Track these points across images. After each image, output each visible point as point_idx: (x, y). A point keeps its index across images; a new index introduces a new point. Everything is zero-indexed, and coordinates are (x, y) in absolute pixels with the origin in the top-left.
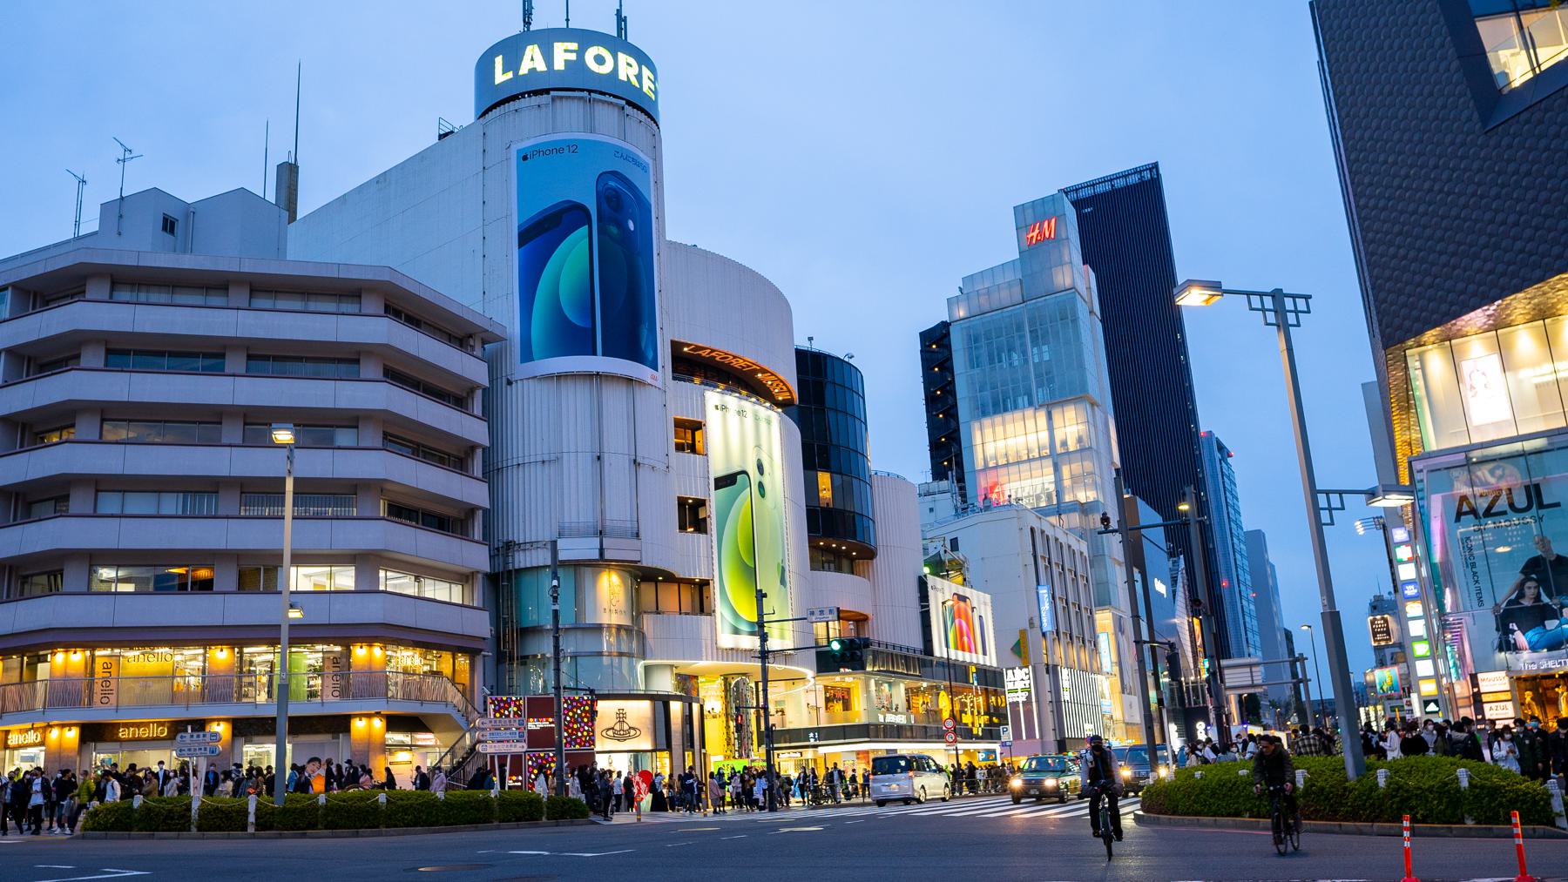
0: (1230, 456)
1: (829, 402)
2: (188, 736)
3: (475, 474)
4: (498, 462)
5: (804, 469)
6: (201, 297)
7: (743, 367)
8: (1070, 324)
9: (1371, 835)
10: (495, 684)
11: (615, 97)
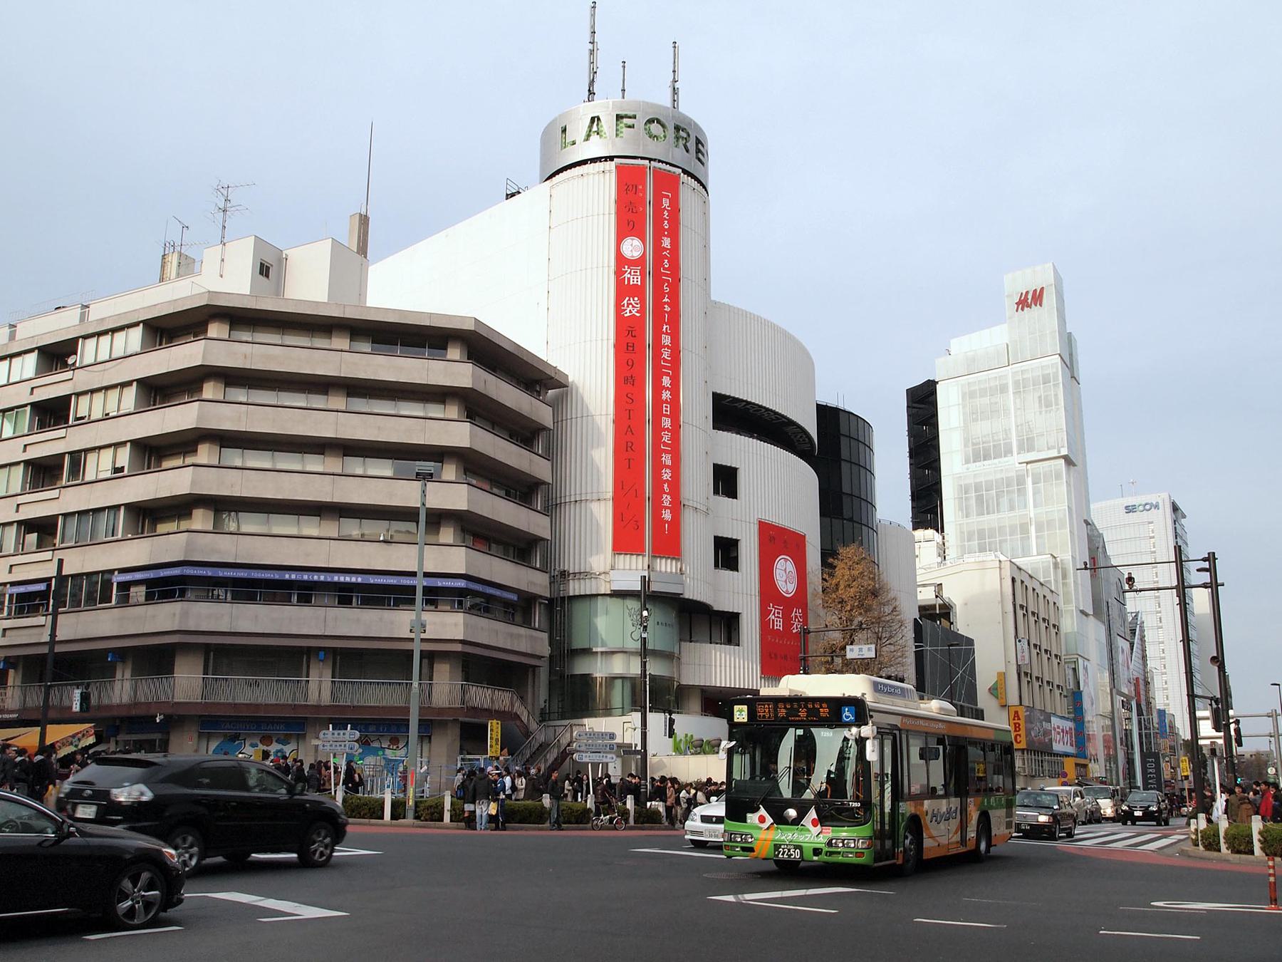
0: (1184, 517)
1: (845, 453)
2: (347, 734)
3: (539, 508)
4: (552, 499)
5: (822, 515)
6: (308, 339)
7: (773, 420)
8: (1052, 388)
9: (434, 828)
10: (548, 699)
11: (671, 165)
